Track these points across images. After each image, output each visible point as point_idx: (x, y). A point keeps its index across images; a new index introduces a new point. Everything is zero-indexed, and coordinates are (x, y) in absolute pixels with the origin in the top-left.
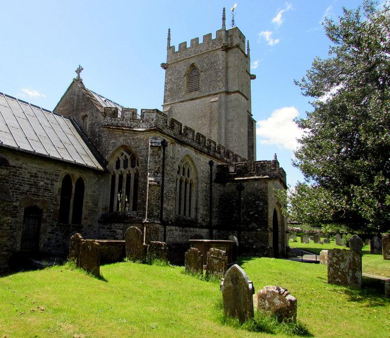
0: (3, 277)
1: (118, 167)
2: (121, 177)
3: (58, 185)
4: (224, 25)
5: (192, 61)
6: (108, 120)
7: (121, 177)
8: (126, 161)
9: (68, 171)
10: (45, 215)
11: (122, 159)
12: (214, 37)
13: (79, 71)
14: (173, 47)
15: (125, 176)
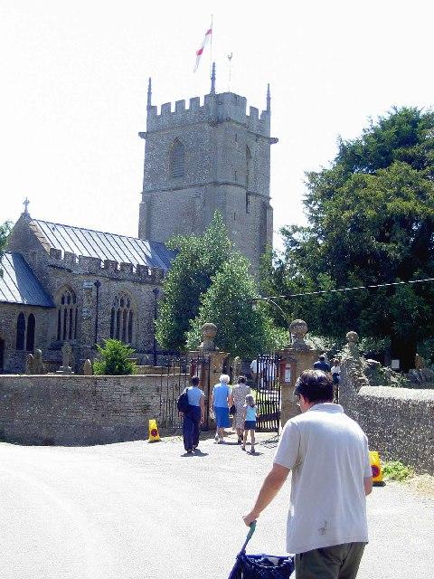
0: (288, 539)
1: (63, 303)
2: (66, 311)
3: (15, 321)
4: (213, 88)
5: (178, 133)
6: (52, 261)
7: (66, 311)
8: (69, 298)
9: (22, 310)
10: (6, 344)
11: (66, 295)
12: (202, 104)
13: (27, 203)
14: (155, 108)
15: (68, 311)
